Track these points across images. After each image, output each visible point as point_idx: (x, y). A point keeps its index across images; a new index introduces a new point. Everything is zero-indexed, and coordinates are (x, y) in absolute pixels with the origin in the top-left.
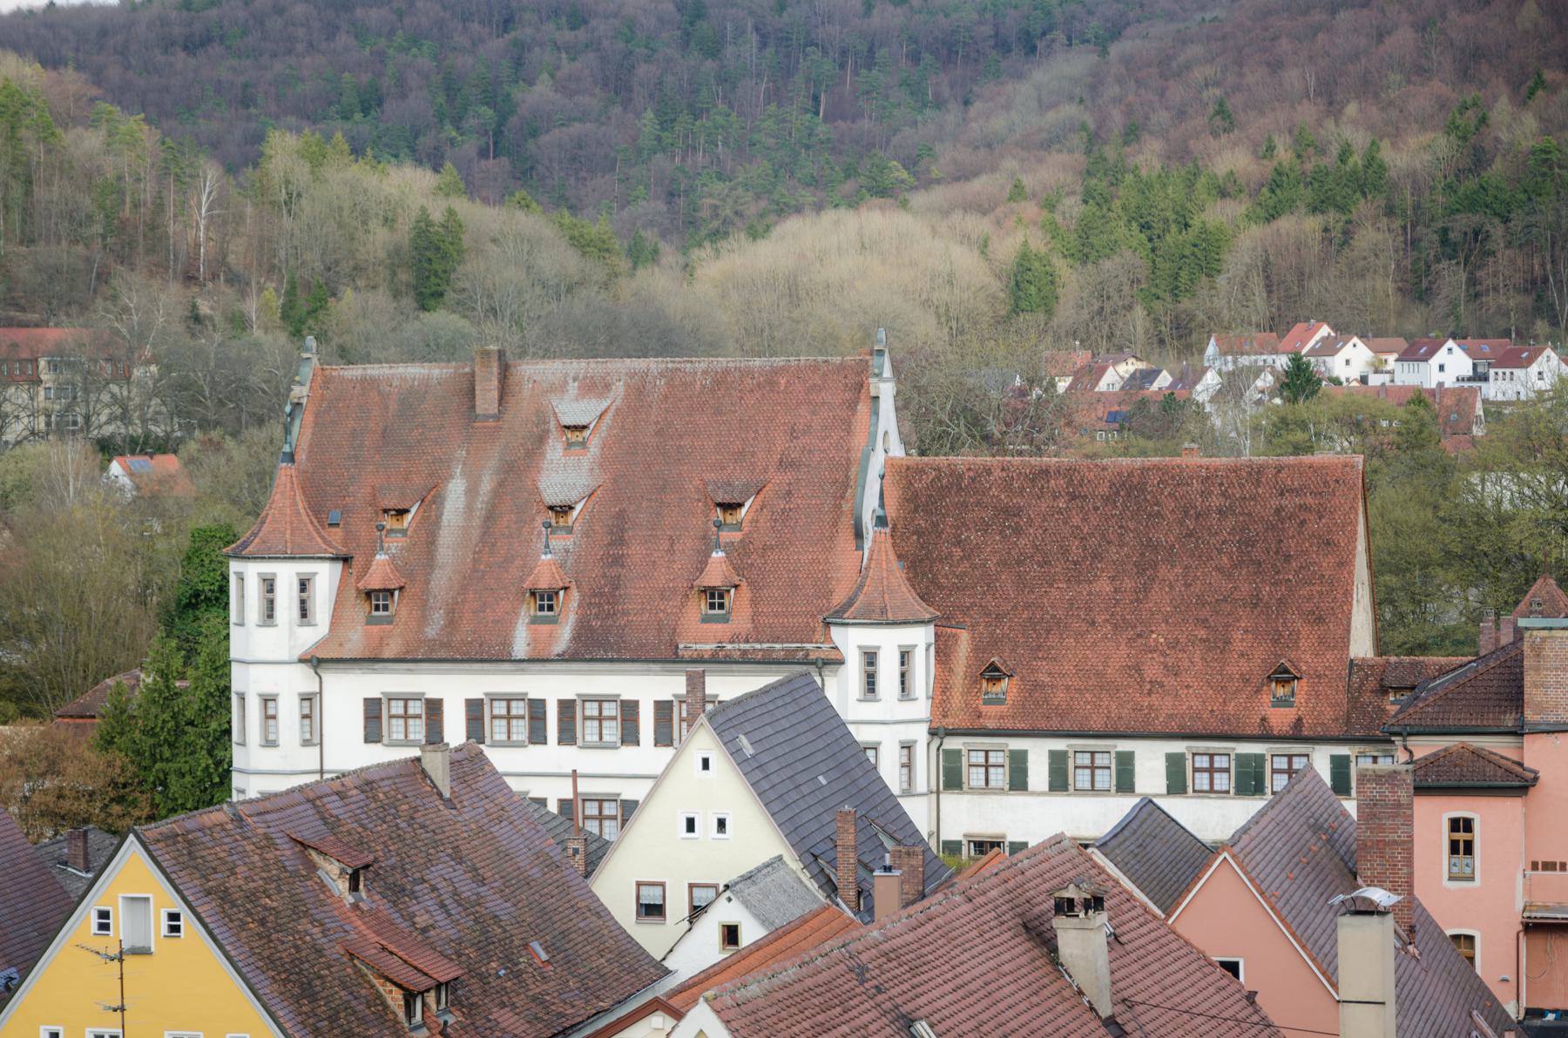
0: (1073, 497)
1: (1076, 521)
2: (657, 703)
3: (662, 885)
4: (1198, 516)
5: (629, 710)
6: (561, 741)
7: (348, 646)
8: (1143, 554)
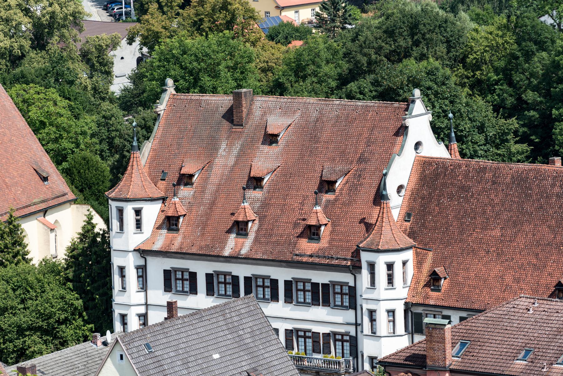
0: (494, 183)
1: (492, 196)
2: (285, 281)
4: (547, 197)
5: (193, 276)
8: (518, 217)
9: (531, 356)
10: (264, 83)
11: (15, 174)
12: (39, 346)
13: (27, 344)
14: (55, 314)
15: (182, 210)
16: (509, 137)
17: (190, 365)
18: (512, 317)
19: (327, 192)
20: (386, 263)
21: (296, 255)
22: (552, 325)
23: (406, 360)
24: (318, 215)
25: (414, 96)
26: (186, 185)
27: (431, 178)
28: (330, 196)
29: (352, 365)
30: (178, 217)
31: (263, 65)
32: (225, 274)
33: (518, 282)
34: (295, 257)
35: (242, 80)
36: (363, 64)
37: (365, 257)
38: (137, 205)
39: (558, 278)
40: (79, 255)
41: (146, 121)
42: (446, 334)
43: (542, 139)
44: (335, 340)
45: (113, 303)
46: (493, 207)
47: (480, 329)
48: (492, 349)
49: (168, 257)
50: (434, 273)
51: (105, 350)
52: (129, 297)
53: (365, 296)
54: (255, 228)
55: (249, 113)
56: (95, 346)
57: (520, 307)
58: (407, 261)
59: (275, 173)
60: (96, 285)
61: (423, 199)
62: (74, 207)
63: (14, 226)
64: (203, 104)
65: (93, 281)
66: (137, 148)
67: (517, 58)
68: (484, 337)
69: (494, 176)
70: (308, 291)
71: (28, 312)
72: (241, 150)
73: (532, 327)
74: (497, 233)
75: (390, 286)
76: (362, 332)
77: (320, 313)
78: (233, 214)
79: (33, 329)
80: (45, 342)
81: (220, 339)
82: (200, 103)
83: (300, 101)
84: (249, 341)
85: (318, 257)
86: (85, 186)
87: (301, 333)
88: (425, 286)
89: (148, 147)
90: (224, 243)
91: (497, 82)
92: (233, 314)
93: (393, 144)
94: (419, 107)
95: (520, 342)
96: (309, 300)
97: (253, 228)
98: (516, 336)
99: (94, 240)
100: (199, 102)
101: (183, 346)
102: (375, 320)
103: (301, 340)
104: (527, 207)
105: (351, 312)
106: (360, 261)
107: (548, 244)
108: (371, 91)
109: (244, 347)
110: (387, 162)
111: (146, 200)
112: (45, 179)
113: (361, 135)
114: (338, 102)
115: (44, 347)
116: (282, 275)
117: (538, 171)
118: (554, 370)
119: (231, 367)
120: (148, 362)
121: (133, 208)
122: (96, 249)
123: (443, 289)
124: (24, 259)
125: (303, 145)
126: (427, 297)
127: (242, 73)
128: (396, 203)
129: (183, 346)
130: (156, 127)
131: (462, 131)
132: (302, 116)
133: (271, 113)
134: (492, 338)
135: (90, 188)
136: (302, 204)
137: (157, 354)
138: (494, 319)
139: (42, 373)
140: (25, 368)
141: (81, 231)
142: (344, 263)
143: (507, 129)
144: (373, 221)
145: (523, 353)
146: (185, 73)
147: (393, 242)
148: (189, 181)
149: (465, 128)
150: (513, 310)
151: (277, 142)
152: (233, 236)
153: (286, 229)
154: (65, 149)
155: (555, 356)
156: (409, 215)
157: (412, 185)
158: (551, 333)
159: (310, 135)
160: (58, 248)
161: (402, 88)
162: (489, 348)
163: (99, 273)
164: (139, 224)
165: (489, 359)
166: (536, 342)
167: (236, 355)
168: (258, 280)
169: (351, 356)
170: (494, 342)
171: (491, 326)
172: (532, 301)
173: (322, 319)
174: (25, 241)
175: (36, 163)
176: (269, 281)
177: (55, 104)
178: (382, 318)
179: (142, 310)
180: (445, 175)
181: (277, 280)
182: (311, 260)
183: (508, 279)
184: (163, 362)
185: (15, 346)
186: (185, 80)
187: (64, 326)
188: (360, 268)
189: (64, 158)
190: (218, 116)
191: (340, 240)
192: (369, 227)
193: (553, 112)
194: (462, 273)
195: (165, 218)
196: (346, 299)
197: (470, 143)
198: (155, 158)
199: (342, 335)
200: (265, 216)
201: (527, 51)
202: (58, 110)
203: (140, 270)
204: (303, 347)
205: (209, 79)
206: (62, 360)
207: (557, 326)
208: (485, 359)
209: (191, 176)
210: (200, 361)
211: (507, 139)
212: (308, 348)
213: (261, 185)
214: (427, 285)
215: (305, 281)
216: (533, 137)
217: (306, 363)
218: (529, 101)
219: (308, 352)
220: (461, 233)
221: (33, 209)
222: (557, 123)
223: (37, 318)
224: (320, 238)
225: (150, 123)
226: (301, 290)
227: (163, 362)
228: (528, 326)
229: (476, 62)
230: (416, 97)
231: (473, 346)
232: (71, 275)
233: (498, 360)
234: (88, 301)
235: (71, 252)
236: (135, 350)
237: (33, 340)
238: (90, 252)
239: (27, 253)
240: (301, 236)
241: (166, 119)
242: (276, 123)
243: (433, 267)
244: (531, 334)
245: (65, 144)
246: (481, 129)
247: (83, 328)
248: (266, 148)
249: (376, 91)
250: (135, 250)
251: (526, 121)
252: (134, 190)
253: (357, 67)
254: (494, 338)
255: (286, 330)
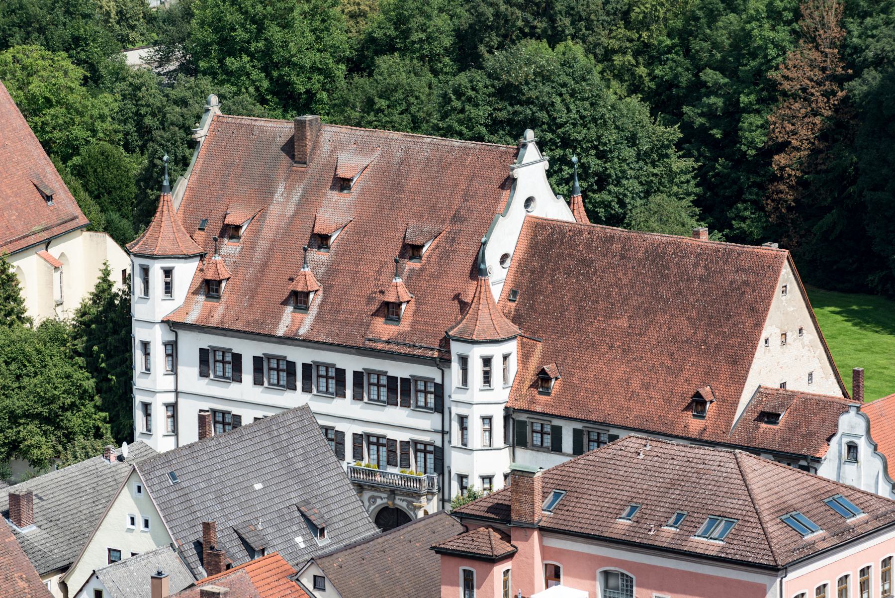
0: (623, 257)
1: (620, 275)
2: (354, 372)
3: (120, 551)
4: (688, 280)
5: (237, 359)
6: (304, 390)
7: (839, 358)
9: (637, 514)
10: (354, 34)
11: (9, 191)
12: (37, 438)
13: (21, 436)
14: (59, 398)
15: (224, 273)
16: (669, 151)
17: (225, 498)
18: (618, 463)
19: (411, 258)
20: (481, 357)
21: (369, 340)
22: (666, 476)
23: (487, 512)
24: (398, 289)
25: (525, 139)
26: (231, 238)
27: (544, 246)
28: (414, 265)
29: (436, 484)
30: (220, 282)
31: (353, 8)
32: (279, 359)
33: (647, 389)
34: (367, 343)
35: (323, 31)
36: (488, 19)
37: (456, 348)
38: (167, 264)
39: (697, 386)
40: (92, 321)
41: (185, 119)
42: (535, 483)
43: (726, 134)
44: (416, 451)
45: (134, 387)
46: (621, 288)
47: (578, 475)
48: (591, 502)
49: (206, 333)
50: (543, 371)
51: (120, 466)
52: (155, 381)
53: (455, 397)
54: (318, 300)
55: (315, 146)
56: (107, 462)
57: (628, 449)
58: (509, 355)
59: (346, 229)
60: (112, 361)
61: (533, 272)
62: (86, 234)
63: (7, 275)
64: (256, 132)
65: (109, 356)
66: (168, 188)
67: (697, 19)
68: (583, 486)
69: (623, 248)
70: (384, 386)
71: (23, 393)
72: (303, 196)
73: (641, 477)
74: (624, 323)
75: (488, 383)
76: (450, 442)
77: (397, 415)
78: (291, 279)
79: (31, 416)
80: (45, 433)
81: (264, 464)
82: (252, 130)
83: (381, 135)
84: (300, 465)
85: (397, 344)
86: (103, 191)
87: (374, 440)
88: (531, 386)
89: (183, 185)
90: (277, 318)
91: (670, 50)
92: (282, 431)
93: (497, 200)
94: (531, 152)
95: (625, 495)
96: (384, 397)
97: (315, 301)
98: (621, 488)
99: (111, 303)
100: (251, 128)
101: (217, 474)
102: (466, 429)
103: (374, 448)
104: (663, 291)
105: (437, 417)
106: (449, 352)
107: (687, 341)
108: (486, 87)
109: (295, 473)
110: (488, 226)
111: (179, 258)
112: (49, 198)
113: (456, 185)
114: (429, 140)
115: (43, 439)
116: (351, 364)
117: (678, 245)
118: (662, 534)
119: (277, 500)
120: (172, 496)
121: (162, 268)
122: (113, 315)
123: (553, 392)
124: (19, 318)
125: (383, 194)
126: (533, 401)
127: (323, 21)
128: (498, 279)
129: (217, 474)
130: (194, 159)
131: (605, 144)
132: (382, 156)
133: (342, 149)
134: (592, 488)
135: (109, 193)
136: (379, 272)
137: (184, 485)
138: (597, 464)
139: (40, 498)
140: (18, 496)
141: (94, 291)
142: (429, 353)
143: (668, 140)
144: (468, 300)
145: (628, 509)
146: (246, 20)
147: (492, 331)
148: (235, 233)
149: (609, 141)
150: (620, 452)
151: (349, 188)
152: (289, 309)
153: (357, 305)
154: (77, 139)
155: (666, 515)
156: (514, 293)
157: (520, 254)
158: (664, 485)
159: (391, 181)
160: (64, 289)
161: (527, 83)
162: (587, 501)
163: (116, 347)
164: (168, 288)
165: (587, 516)
166: (644, 496)
167: (284, 485)
168: (320, 368)
169: (435, 471)
170: (594, 493)
171: (592, 473)
172: (644, 442)
173: (402, 422)
174: (22, 295)
175: (38, 178)
176: (334, 370)
177: (66, 73)
178: (475, 426)
179: (171, 398)
180: (562, 243)
181: (344, 370)
182: (387, 347)
183: (635, 384)
184: (191, 496)
185: (6, 438)
186: (246, 30)
187: (69, 414)
188: (450, 361)
189: (76, 151)
190: (276, 149)
191: (426, 323)
192: (464, 306)
193: (741, 99)
194: (578, 374)
195: (202, 283)
196: (431, 399)
197: (616, 160)
198: (193, 200)
199: (426, 444)
200: (331, 286)
201: (712, 11)
202: (70, 84)
203: (169, 347)
204: (376, 457)
205: (278, 29)
206: (66, 481)
207: (671, 476)
208: (582, 515)
209: (238, 227)
210: (238, 494)
211: (667, 154)
212: (381, 458)
213: (327, 244)
214: (534, 385)
215: (379, 374)
216: (714, 131)
217: (378, 479)
218: (710, 84)
219: (381, 463)
220: (579, 320)
221: (32, 240)
222: (745, 115)
223: (35, 402)
224: (399, 319)
225: (190, 122)
226: (374, 384)
227: (191, 496)
228: (636, 475)
229: (644, 17)
230: (528, 140)
231: (568, 498)
232: (80, 348)
233: (597, 518)
234: (101, 381)
235: (82, 317)
236: (156, 481)
237: (31, 434)
238: (105, 317)
239: (24, 311)
240: (376, 314)
241: (208, 149)
242: (349, 163)
243: (542, 363)
244: (639, 486)
245: (79, 132)
246: (632, 140)
247: (94, 416)
248: (334, 195)
249: (493, 86)
250: (162, 322)
251: (705, 110)
252: (164, 244)
253: (480, 21)
254: (595, 488)
255: (354, 434)
